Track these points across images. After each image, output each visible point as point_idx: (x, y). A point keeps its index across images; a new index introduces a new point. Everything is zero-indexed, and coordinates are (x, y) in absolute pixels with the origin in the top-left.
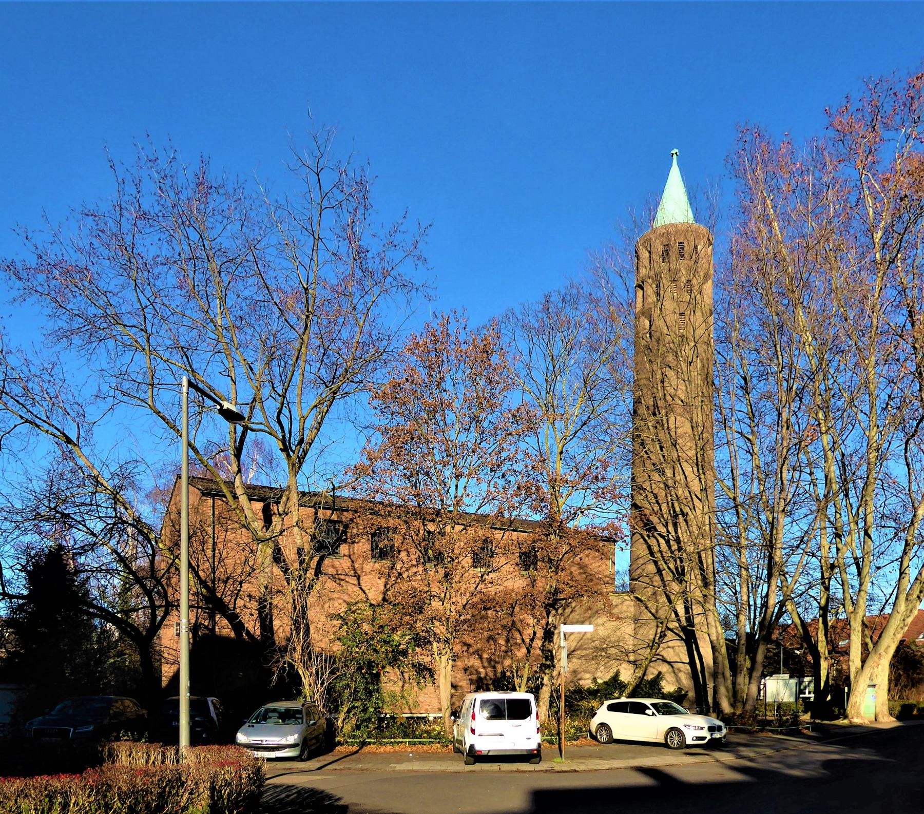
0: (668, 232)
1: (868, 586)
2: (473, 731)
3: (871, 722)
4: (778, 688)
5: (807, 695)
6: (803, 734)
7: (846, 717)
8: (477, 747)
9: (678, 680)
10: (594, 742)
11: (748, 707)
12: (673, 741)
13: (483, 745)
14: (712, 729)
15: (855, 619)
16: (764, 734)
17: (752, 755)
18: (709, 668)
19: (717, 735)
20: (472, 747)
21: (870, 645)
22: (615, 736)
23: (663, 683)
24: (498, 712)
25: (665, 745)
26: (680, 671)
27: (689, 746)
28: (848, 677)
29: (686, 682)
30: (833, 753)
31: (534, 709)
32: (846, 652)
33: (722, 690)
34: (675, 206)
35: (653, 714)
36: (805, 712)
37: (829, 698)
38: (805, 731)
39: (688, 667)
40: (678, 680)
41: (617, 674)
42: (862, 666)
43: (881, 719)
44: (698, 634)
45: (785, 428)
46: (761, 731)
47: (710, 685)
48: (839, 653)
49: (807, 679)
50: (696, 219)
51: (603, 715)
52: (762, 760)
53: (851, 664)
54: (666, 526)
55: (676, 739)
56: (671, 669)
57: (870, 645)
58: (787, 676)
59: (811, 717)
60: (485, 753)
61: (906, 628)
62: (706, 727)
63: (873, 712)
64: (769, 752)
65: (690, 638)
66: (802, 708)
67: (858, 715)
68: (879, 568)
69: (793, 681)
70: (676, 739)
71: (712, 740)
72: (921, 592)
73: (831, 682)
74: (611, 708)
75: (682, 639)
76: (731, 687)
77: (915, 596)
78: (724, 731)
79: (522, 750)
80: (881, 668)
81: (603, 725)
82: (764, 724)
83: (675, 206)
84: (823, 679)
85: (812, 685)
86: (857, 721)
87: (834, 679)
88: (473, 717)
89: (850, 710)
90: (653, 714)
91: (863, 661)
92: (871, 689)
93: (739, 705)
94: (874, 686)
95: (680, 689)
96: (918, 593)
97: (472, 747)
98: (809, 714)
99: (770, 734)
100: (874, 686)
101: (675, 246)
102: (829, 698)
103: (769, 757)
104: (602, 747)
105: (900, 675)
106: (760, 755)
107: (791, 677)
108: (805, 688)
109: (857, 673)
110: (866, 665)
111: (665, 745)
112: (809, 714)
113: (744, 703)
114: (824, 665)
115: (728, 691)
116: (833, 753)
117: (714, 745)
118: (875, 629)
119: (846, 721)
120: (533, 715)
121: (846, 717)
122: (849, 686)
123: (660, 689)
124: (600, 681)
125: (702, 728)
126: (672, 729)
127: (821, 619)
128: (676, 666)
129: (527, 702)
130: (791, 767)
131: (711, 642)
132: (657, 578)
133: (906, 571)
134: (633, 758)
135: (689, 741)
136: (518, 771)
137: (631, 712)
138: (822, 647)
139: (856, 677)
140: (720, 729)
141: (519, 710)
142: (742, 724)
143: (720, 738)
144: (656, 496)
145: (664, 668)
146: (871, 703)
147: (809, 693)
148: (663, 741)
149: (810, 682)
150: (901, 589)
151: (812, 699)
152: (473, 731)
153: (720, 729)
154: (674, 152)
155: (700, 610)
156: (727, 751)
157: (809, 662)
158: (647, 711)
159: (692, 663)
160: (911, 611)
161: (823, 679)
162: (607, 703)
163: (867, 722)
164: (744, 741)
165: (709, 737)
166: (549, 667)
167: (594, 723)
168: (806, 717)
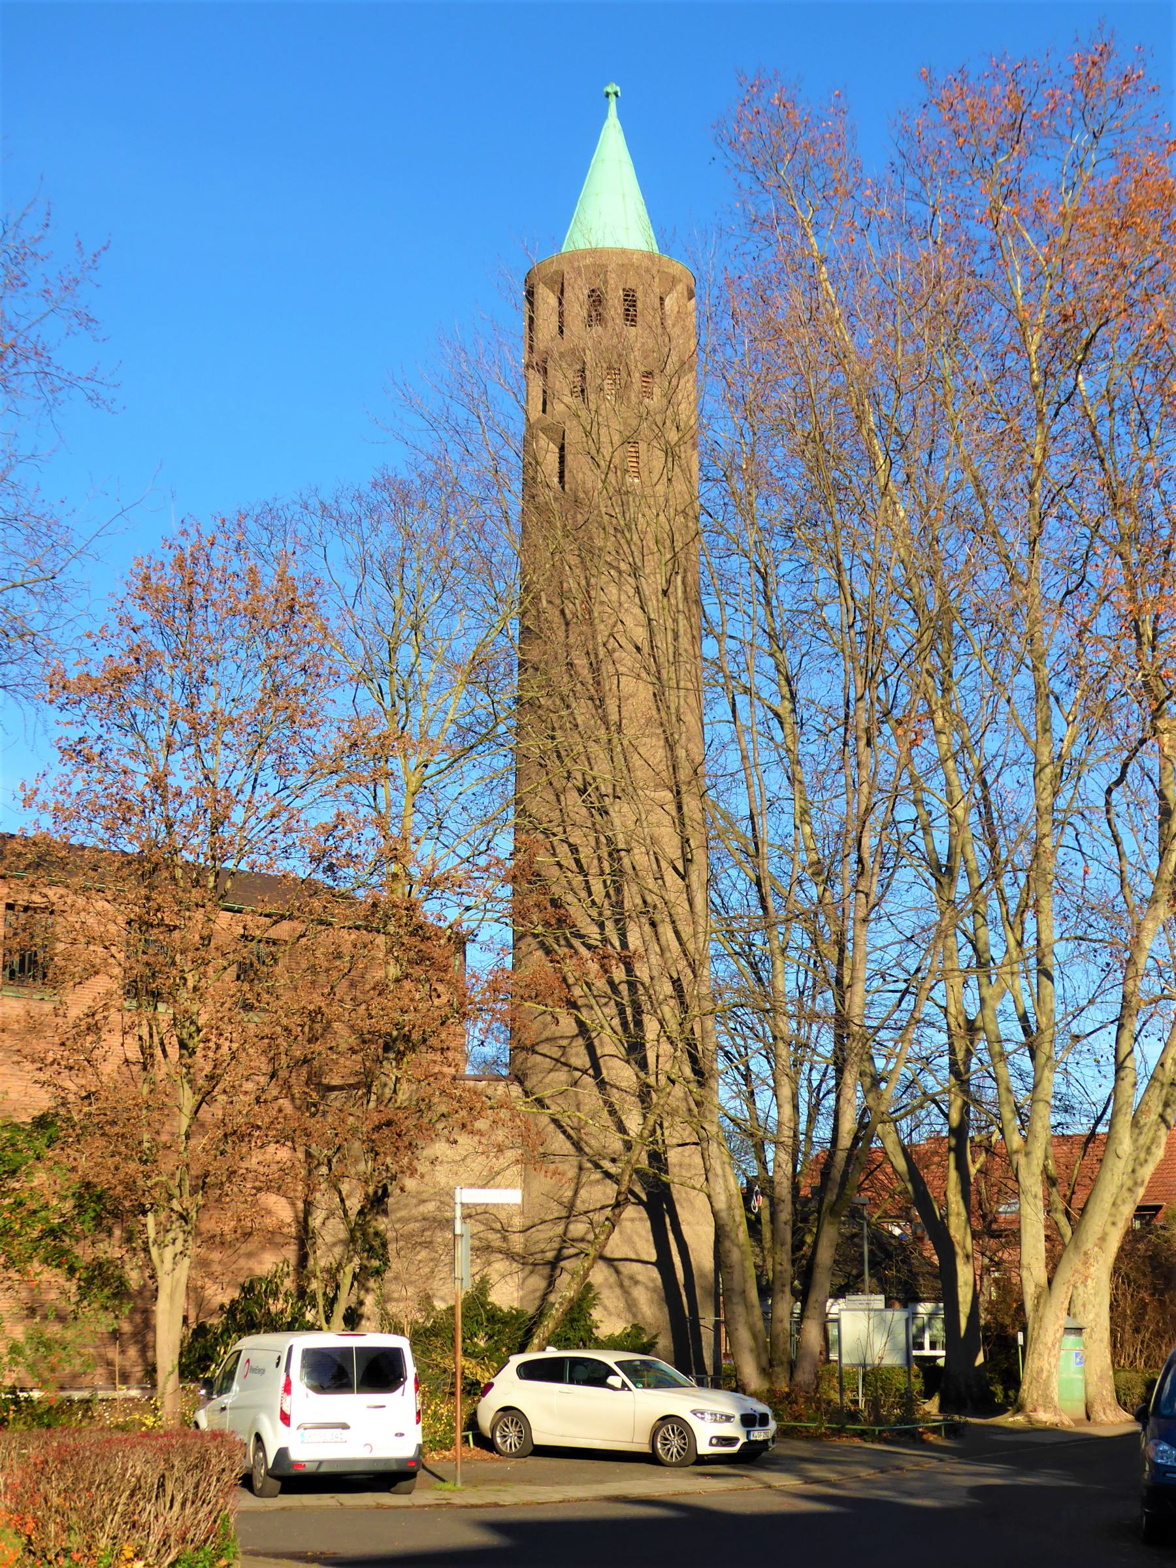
0: (598, 263)
1: (1053, 1081)
2: (285, 1418)
3: (1077, 1422)
4: (862, 1329)
5: (927, 1352)
6: (923, 1441)
7: (1020, 1409)
8: (295, 1455)
9: (631, 1305)
10: (486, 1454)
11: (804, 1375)
12: (668, 1443)
13: (309, 1449)
14: (748, 1421)
15: (1029, 1164)
16: (845, 1442)
17: (833, 1477)
18: (703, 1275)
19: (758, 1435)
20: (282, 1453)
21: (1067, 1230)
22: (539, 1439)
23: (596, 1314)
24: (332, 1373)
25: (650, 1458)
26: (637, 1283)
27: (702, 1460)
28: (1021, 1308)
29: (651, 1311)
30: (991, 1476)
31: (411, 1370)
32: (1012, 1236)
33: (744, 1336)
34: (613, 212)
35: (624, 1385)
36: (928, 1395)
37: (980, 1359)
38: (932, 1438)
39: (655, 1273)
40: (631, 1305)
41: (483, 1287)
42: (1050, 1282)
43: (1099, 1415)
44: (677, 1192)
45: (864, 741)
46: (838, 1432)
47: (707, 1319)
48: (997, 1234)
49: (924, 1308)
50: (664, 246)
51: (508, 1388)
52: (853, 1485)
53: (1025, 1274)
54: (602, 926)
55: (676, 1442)
56: (613, 1279)
57: (1067, 1230)
58: (879, 1301)
59: (942, 1409)
60: (310, 1468)
61: (1141, 1192)
62: (738, 1417)
63: (1079, 1394)
64: (864, 1473)
65: (660, 1205)
66: (918, 1385)
67: (1048, 1403)
68: (1077, 1038)
69: (897, 1316)
70: (676, 1442)
71: (749, 1444)
72: (1166, 1105)
73: (984, 1318)
74: (530, 1371)
75: (640, 1202)
76: (760, 1325)
77: (1154, 1117)
78: (773, 1425)
79: (387, 1461)
80: (1092, 1284)
81: (509, 1412)
82: (844, 1418)
83: (613, 212)
84: (964, 1309)
85: (939, 1324)
86: (1044, 1417)
87: (992, 1307)
88: (287, 1388)
89: (1029, 1392)
90: (624, 1385)
91: (1054, 1263)
92: (1071, 1339)
93: (781, 1373)
94: (1078, 1330)
95: (638, 1329)
96: (1160, 1109)
97: (282, 1453)
98: (936, 1400)
99: (857, 1442)
100: (1078, 1330)
101: (613, 296)
102: (980, 1359)
103: (866, 1481)
104: (511, 1464)
105: (1144, 1305)
106: (855, 1473)
107: (888, 1305)
108: (922, 1330)
109: (1038, 1298)
110: (1054, 1284)
111: (650, 1458)
112: (936, 1400)
113: (793, 1366)
114: (965, 1274)
115: (755, 1337)
116: (991, 1476)
117: (750, 1457)
118: (1071, 1194)
119: (1020, 1418)
120: (410, 1383)
121: (1020, 1409)
122: (1024, 1329)
123: (590, 1331)
124: (440, 1305)
125: (728, 1418)
126: (665, 1419)
127: (952, 1156)
128: (627, 1268)
129: (394, 1355)
130: (911, 1494)
131: (715, 1214)
132: (579, 1045)
133: (1128, 1063)
134: (601, 1482)
135: (704, 1448)
136: (379, 1507)
137: (571, 1382)
138: (958, 1229)
139: (1037, 1307)
140: (763, 1420)
141: (380, 1372)
142: (796, 1419)
143: (765, 1442)
144: (574, 849)
145: (599, 1275)
146: (1071, 1376)
147: (933, 1346)
148: (646, 1449)
149: (932, 1315)
150: (1121, 1101)
151: (941, 1362)
152: (285, 1418)
153: (763, 1420)
154: (609, 89)
155: (688, 1135)
156: (780, 1471)
157: (931, 1264)
158: (611, 1380)
159: (664, 1264)
160: (1148, 1150)
161: (964, 1309)
162: (516, 1360)
163: (1067, 1421)
164: (807, 1455)
165: (743, 1440)
166: (378, 1272)
167: (488, 1408)
168: (932, 1406)
